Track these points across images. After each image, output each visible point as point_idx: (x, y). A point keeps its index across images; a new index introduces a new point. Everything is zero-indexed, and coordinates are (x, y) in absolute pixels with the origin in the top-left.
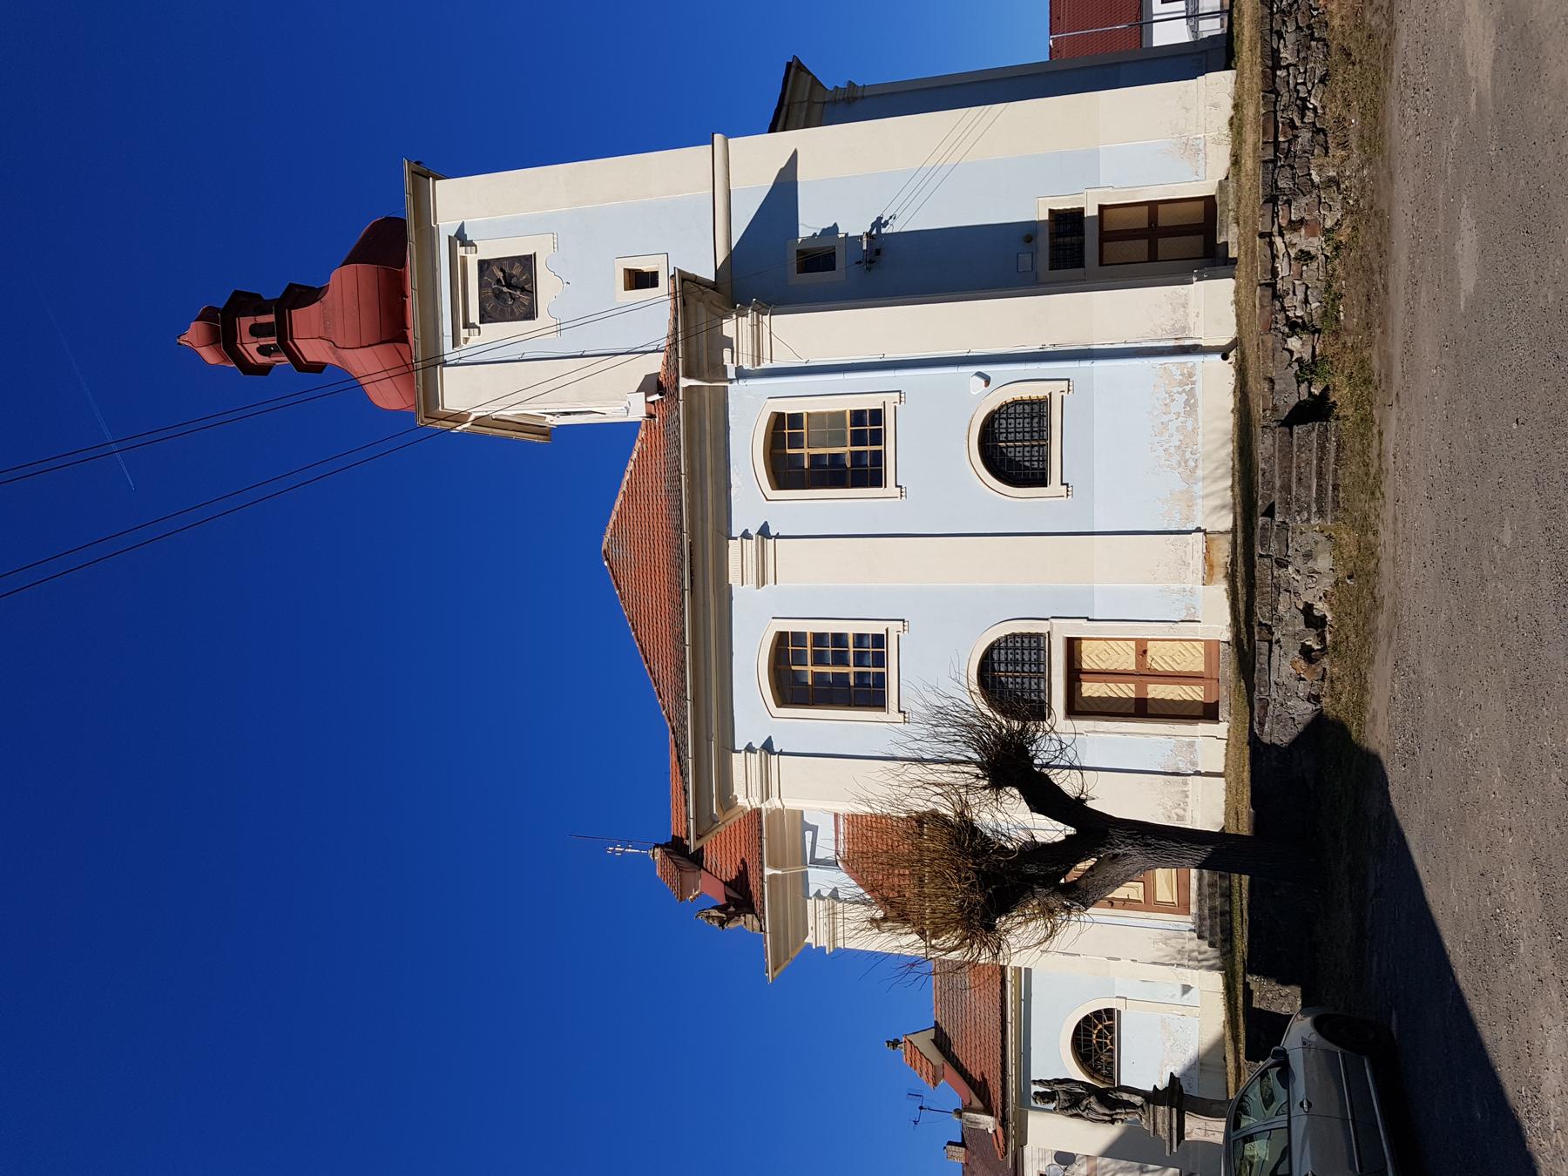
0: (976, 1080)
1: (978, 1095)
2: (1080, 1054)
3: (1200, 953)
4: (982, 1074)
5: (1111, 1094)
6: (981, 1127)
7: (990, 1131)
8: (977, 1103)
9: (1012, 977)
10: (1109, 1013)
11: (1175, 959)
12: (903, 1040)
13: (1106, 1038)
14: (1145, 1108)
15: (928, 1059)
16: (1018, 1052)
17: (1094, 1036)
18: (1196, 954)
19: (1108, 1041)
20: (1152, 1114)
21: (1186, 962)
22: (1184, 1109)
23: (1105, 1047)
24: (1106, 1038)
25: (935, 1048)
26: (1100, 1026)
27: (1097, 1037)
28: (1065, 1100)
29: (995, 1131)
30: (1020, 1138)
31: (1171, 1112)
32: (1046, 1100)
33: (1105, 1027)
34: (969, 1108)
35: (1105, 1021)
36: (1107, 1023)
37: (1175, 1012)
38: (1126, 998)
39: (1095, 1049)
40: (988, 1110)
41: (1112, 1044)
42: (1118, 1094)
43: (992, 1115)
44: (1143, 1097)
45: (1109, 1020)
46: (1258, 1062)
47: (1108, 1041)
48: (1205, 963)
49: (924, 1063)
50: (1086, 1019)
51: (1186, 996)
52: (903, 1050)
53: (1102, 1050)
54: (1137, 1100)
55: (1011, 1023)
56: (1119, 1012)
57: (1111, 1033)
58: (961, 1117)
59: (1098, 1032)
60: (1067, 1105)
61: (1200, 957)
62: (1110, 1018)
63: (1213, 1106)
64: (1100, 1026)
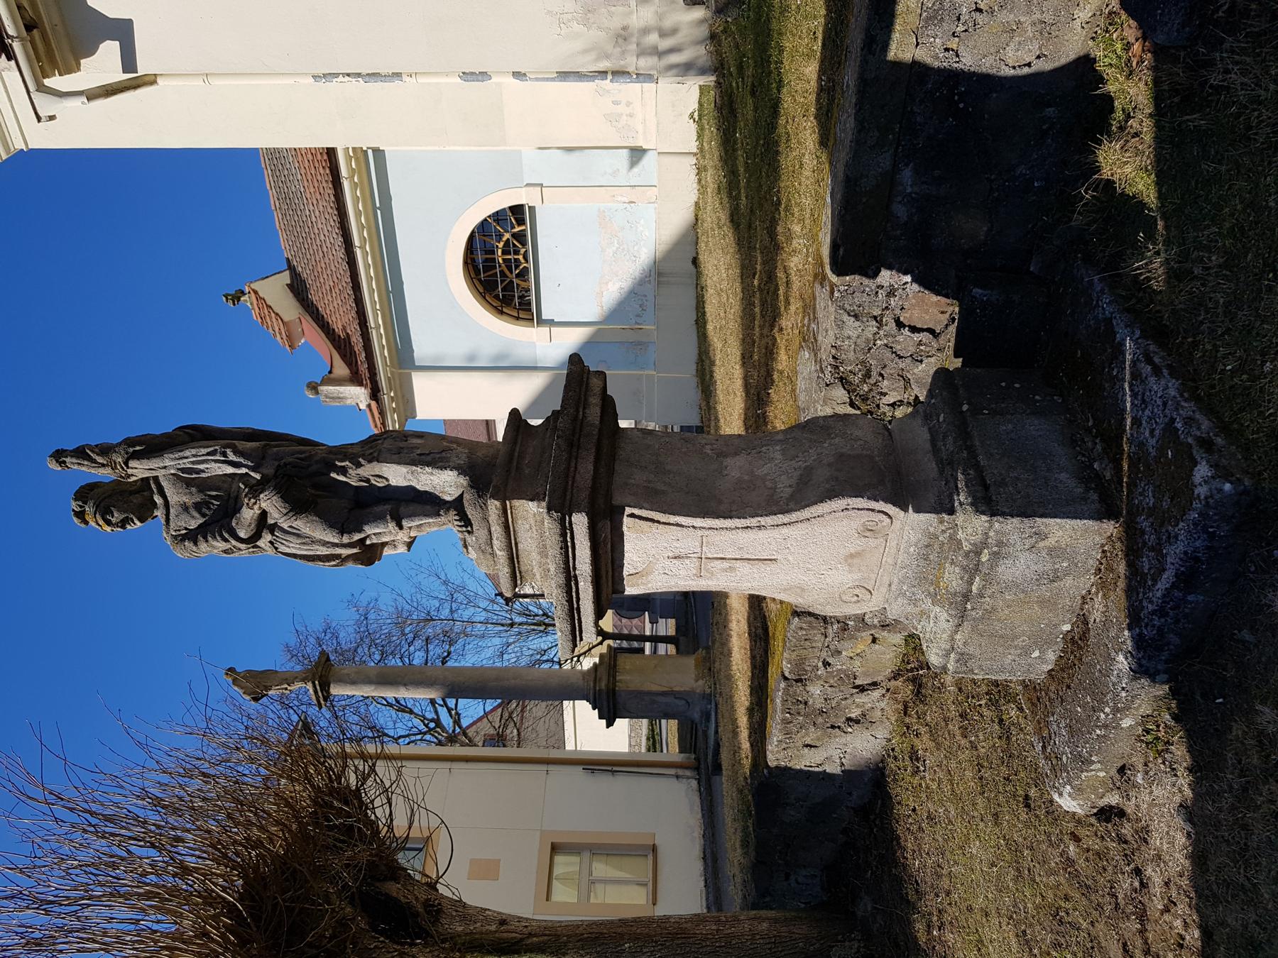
0: (339, 336)
1: (343, 357)
2: (480, 280)
3: (663, 34)
4: (344, 328)
5: (344, 471)
6: (349, 402)
7: (363, 406)
8: (341, 369)
9: (352, 172)
10: (517, 210)
11: (607, 57)
12: (247, 291)
13: (517, 252)
14: (471, 512)
15: (277, 314)
16: (384, 292)
17: (500, 251)
18: (653, 38)
19: (521, 257)
20: (497, 530)
21: (631, 63)
22: (617, 501)
23: (517, 267)
24: (517, 252)
25: (291, 295)
26: (507, 236)
27: (503, 253)
28: (185, 508)
29: (369, 406)
30: (405, 410)
31: (565, 531)
32: (117, 517)
33: (514, 235)
34: (330, 380)
35: (513, 227)
36: (517, 229)
37: (620, 198)
38: (541, 185)
39: (502, 272)
40: (355, 379)
41: (526, 260)
42: (368, 470)
43: (360, 384)
44: (462, 470)
45: (519, 225)
46: (875, 275)
47: (521, 257)
48: (675, 59)
49: (274, 320)
50: (483, 225)
51: (636, 170)
52: (248, 304)
53: (511, 273)
54: (445, 483)
55: (362, 247)
56: (532, 209)
57: (524, 244)
58: (317, 393)
59: (504, 246)
60: (193, 524)
61: (665, 44)
62: (521, 222)
63: (729, 461)
64: (507, 236)
